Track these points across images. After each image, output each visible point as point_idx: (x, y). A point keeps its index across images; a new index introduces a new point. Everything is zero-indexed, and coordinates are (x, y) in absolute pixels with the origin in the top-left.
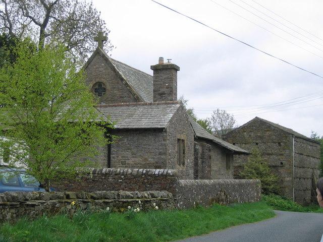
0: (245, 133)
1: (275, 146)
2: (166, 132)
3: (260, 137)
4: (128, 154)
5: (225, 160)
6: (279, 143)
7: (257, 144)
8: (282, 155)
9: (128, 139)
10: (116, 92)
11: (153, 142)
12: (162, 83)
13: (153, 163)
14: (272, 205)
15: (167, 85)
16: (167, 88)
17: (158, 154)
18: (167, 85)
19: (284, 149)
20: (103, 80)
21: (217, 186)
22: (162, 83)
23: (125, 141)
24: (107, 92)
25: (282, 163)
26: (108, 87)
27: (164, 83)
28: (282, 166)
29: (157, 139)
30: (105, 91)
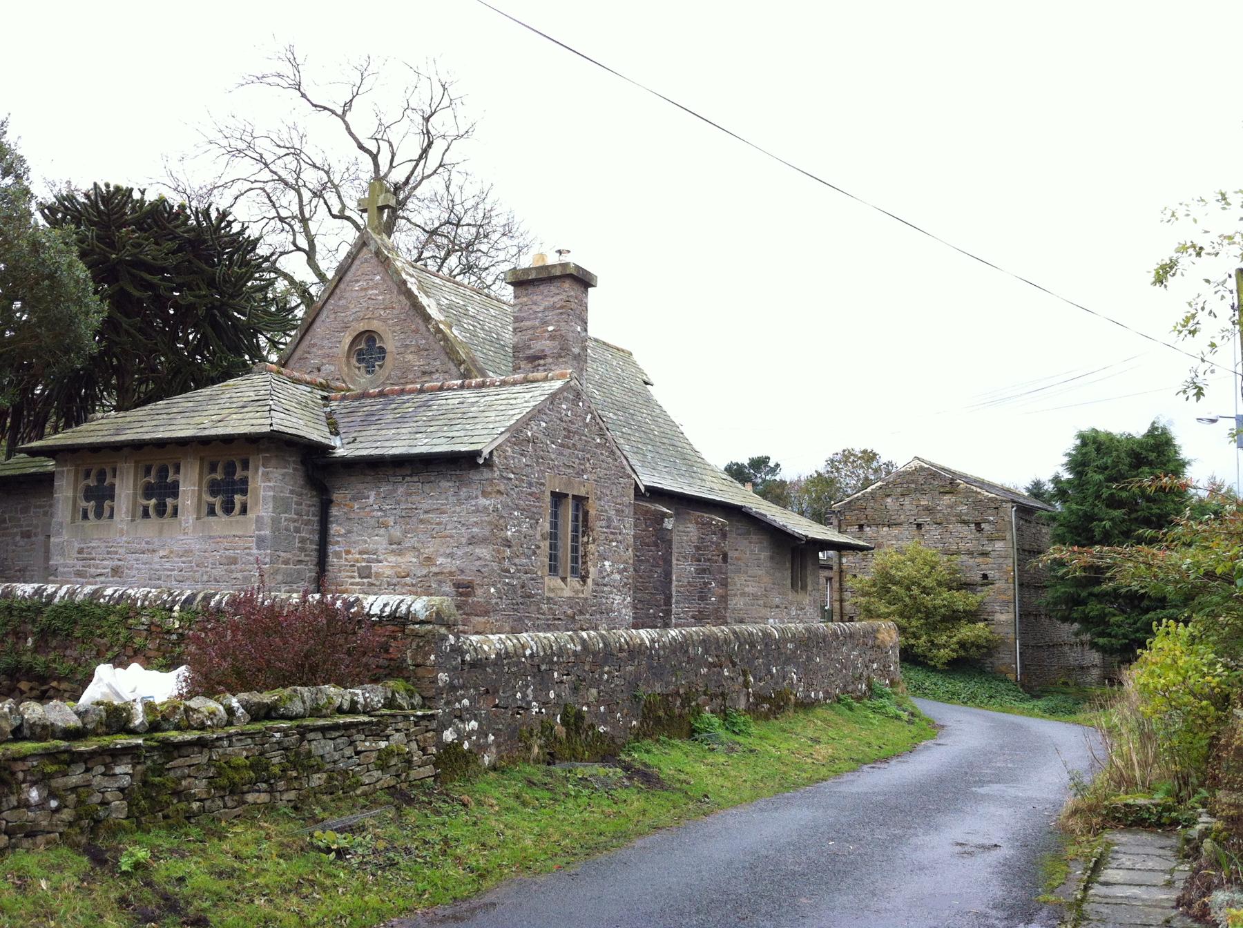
0: (889, 500)
1: (968, 531)
2: (489, 463)
3: (927, 509)
4: (378, 542)
5: (788, 565)
6: (978, 525)
7: (919, 526)
8: (985, 554)
9: (378, 494)
10: (410, 357)
11: (451, 499)
12: (537, 323)
13: (451, 574)
14: (1188, 598)
15: (550, 328)
16: (552, 337)
17: (464, 540)
18: (550, 328)
19: (991, 540)
20: (375, 325)
21: (38, 730)
22: (537, 323)
23: (371, 500)
24: (388, 358)
25: (985, 576)
26: (390, 343)
27: (545, 323)
28: (987, 585)
29: (463, 493)
30: (384, 358)
